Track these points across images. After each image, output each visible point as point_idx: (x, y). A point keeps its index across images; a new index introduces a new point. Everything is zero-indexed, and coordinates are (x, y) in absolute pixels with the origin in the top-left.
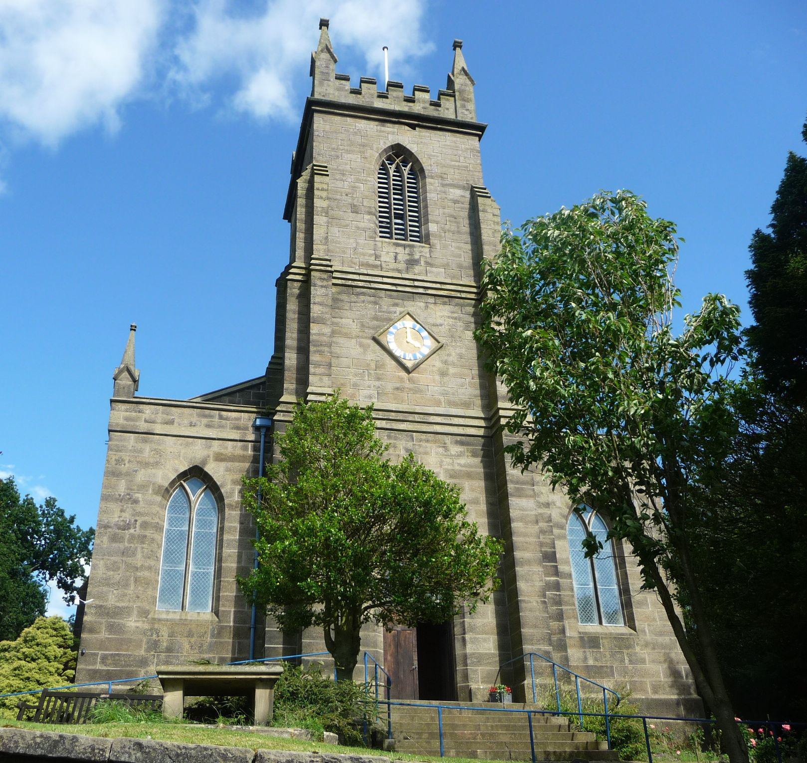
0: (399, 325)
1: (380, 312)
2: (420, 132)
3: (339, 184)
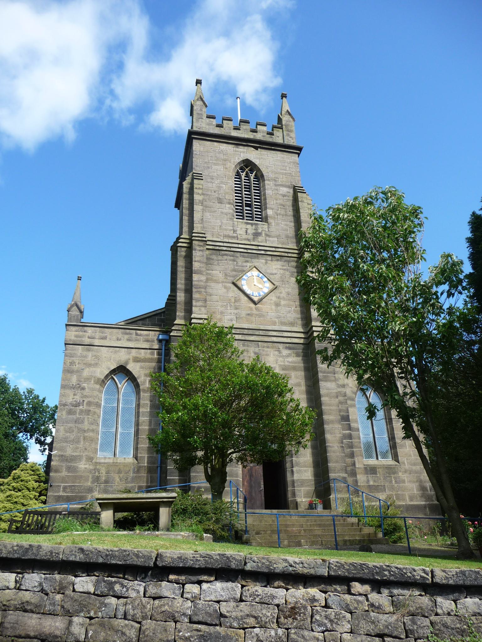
0: (249, 274)
1: (237, 266)
2: (261, 151)
3: (210, 185)
